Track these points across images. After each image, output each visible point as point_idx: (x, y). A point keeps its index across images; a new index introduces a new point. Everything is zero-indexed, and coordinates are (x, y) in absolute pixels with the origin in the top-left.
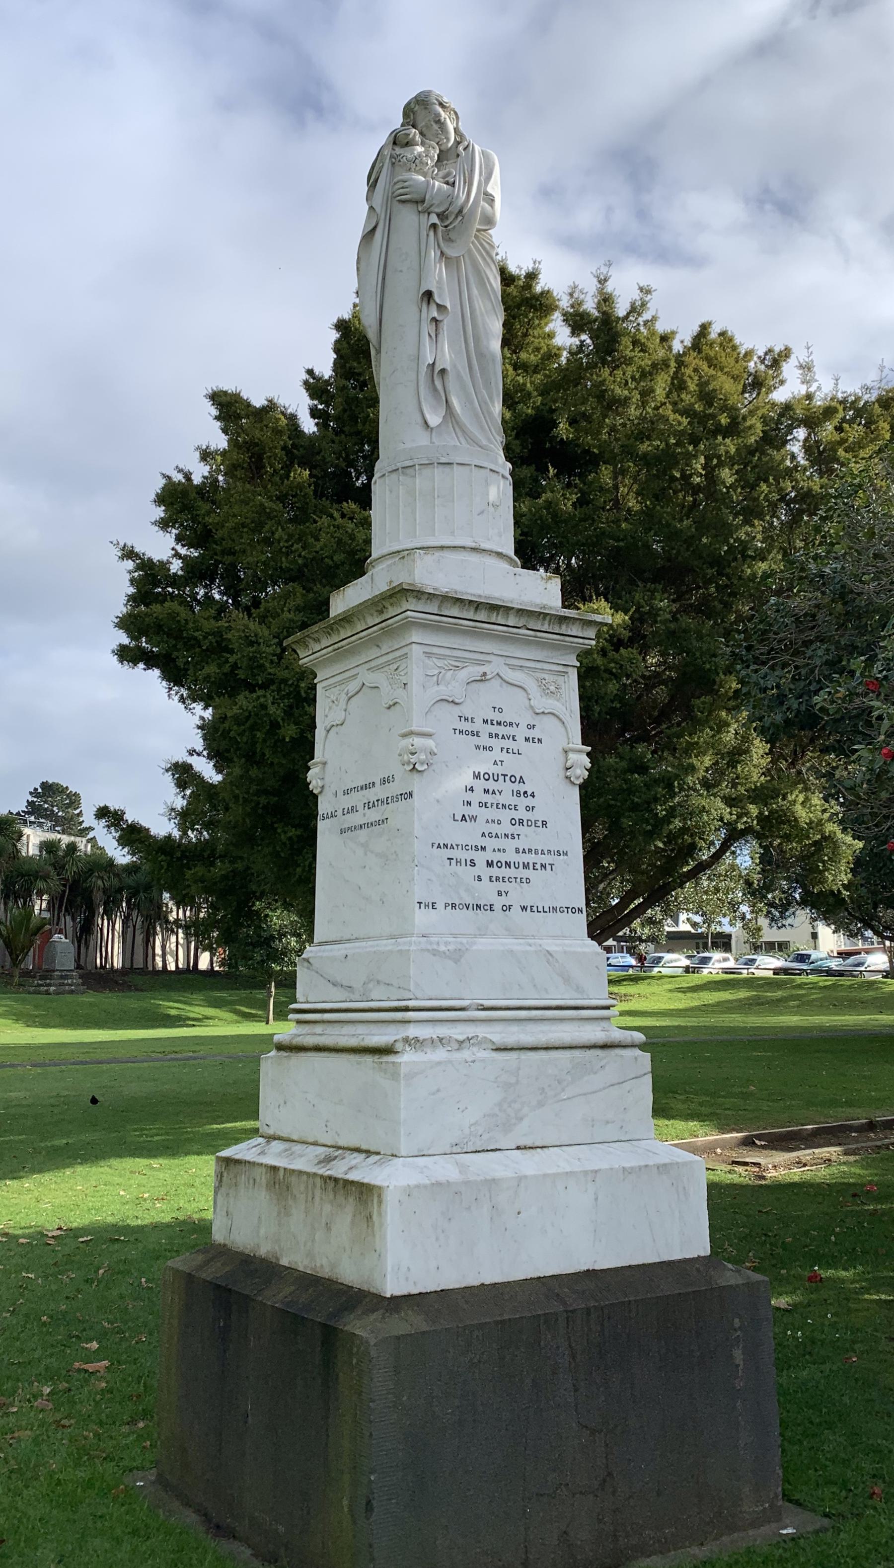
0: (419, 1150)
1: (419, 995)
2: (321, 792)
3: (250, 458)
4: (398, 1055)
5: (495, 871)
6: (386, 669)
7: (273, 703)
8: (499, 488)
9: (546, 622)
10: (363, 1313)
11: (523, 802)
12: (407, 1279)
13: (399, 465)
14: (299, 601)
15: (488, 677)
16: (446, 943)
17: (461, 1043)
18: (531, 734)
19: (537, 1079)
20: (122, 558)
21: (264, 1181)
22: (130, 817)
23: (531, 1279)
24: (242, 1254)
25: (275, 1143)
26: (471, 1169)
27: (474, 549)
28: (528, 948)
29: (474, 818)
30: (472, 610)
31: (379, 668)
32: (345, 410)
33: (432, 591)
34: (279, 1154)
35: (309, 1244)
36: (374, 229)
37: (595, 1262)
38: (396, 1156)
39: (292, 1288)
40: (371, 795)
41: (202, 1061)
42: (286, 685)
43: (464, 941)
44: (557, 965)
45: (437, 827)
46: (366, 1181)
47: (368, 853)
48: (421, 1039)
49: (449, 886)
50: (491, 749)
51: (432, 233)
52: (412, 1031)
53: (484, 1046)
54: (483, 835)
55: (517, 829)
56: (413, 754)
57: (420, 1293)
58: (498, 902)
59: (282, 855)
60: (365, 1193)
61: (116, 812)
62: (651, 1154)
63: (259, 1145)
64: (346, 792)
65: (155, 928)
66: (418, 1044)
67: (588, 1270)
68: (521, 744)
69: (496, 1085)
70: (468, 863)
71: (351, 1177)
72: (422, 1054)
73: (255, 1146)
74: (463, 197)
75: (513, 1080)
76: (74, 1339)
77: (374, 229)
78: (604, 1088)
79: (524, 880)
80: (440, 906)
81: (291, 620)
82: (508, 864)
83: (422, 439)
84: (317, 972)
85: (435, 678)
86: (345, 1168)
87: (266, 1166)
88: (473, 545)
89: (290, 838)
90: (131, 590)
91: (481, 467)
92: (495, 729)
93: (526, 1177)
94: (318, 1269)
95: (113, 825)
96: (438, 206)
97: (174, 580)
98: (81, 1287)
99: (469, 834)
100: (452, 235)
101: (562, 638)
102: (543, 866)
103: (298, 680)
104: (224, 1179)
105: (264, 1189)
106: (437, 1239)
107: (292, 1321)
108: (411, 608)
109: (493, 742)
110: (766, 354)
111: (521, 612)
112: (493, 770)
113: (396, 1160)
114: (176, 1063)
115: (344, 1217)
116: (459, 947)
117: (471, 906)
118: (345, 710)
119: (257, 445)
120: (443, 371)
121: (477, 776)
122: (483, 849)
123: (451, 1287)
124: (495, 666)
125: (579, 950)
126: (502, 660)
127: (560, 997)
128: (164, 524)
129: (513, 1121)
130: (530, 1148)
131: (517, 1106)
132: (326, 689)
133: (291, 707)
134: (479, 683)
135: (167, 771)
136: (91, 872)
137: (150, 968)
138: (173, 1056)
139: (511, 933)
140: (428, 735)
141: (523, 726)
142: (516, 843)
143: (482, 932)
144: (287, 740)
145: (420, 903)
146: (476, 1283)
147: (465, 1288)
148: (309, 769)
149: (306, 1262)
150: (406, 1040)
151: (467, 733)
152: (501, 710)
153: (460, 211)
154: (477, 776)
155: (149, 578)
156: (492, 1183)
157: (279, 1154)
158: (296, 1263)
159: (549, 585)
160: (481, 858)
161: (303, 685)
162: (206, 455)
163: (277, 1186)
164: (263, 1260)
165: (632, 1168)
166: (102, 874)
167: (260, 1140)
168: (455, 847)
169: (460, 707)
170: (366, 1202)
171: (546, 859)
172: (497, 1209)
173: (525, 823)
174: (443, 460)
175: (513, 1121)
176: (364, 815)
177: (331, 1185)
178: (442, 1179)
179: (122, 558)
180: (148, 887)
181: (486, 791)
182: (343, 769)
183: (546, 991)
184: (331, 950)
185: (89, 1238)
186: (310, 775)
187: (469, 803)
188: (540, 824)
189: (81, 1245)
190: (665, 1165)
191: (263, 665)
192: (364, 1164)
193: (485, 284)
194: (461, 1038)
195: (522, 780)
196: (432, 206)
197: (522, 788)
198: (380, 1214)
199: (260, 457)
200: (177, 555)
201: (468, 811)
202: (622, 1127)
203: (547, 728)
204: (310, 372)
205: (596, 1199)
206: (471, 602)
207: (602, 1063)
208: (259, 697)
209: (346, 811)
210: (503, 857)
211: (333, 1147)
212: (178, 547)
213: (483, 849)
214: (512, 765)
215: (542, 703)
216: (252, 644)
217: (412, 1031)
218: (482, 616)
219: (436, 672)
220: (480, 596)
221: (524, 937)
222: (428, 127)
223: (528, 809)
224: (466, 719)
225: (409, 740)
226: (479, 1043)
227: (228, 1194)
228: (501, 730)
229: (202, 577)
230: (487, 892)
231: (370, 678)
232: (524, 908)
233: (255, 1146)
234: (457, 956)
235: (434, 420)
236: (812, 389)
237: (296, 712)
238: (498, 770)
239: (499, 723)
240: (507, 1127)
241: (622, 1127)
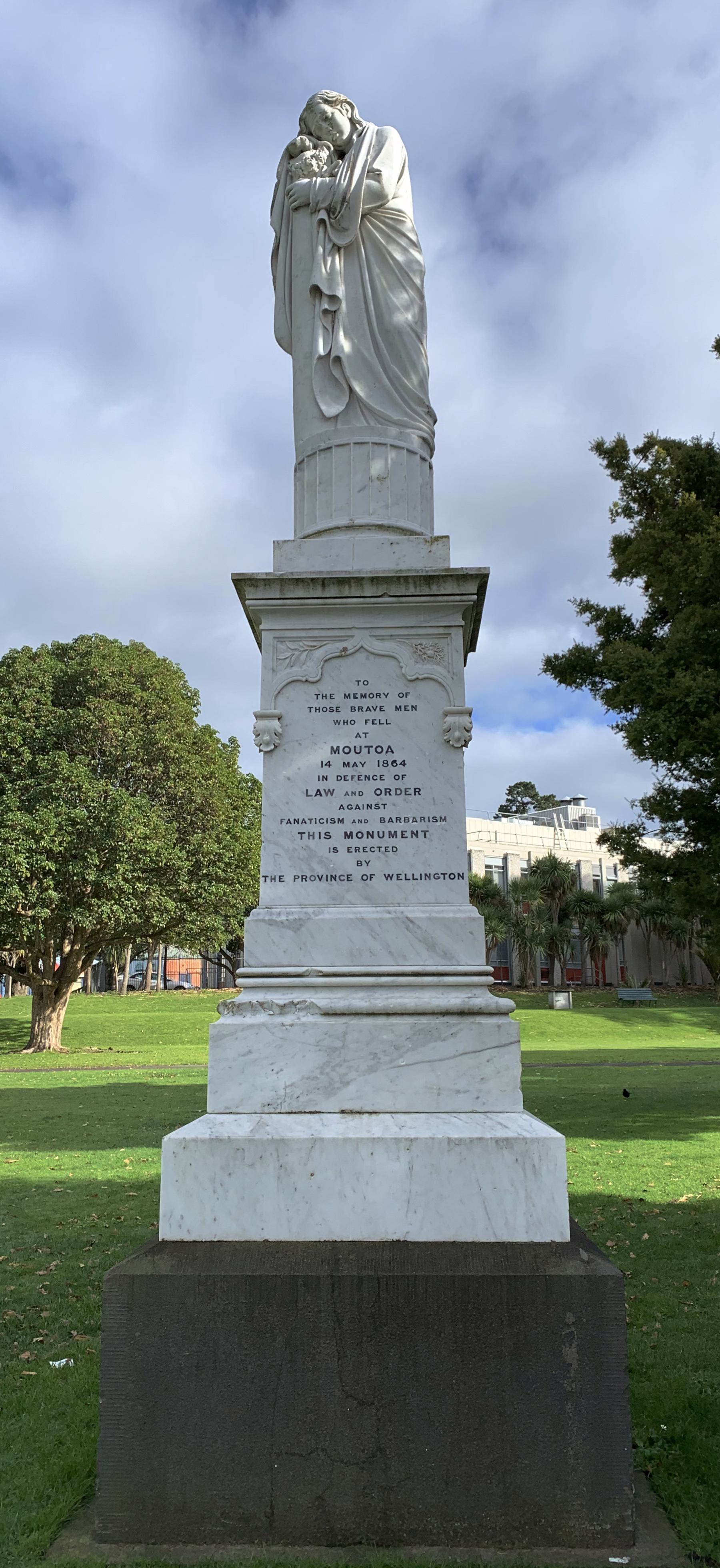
0: (226, 1108)
1: (252, 962)
5: (354, 842)
8: (386, 460)
18: (402, 702)
19: (367, 1044)
23: (325, 1241)
26: (267, 1128)
27: (350, 527)
29: (330, 792)
30: (319, 588)
33: (264, 577)
37: (407, 1233)
42: (675, 703)
44: (419, 931)
45: (287, 803)
49: (300, 859)
50: (352, 722)
51: (321, 230)
53: (312, 1011)
54: (341, 807)
57: (194, 1241)
58: (357, 873)
66: (235, 1009)
67: (398, 1241)
69: (318, 1048)
74: (344, 183)
75: (338, 1044)
78: (455, 1056)
79: (390, 849)
80: (288, 878)
82: (370, 835)
91: (362, 443)
92: (356, 703)
93: (322, 1139)
96: (324, 201)
99: (326, 808)
100: (344, 224)
101: (432, 599)
102: (415, 834)
106: (215, 1192)
109: (356, 715)
111: (375, 580)
112: (354, 742)
117: (325, 877)
121: (335, 751)
122: (341, 821)
123: (230, 1240)
126: (367, 632)
127: (422, 963)
131: (342, 1070)
134: (340, 659)
139: (371, 901)
142: (381, 813)
151: (324, 710)
152: (366, 682)
153: (344, 199)
154: (335, 751)
156: (281, 1144)
168: (308, 822)
169: (318, 685)
171: (419, 827)
172: (286, 1169)
173: (393, 792)
175: (337, 1085)
183: (404, 957)
187: (325, 778)
193: (387, 260)
194: (281, 1002)
195: (390, 749)
196: (317, 203)
197: (390, 758)
201: (322, 786)
202: (478, 1098)
206: (312, 579)
207: (453, 1030)
210: (364, 828)
213: (341, 821)
214: (377, 736)
218: (332, 591)
220: (321, 572)
221: (387, 904)
222: (320, 128)
223: (396, 777)
228: (366, 703)
230: (346, 863)
232: (389, 877)
234: (297, 925)
238: (362, 742)
239: (364, 696)
240: (330, 1090)
241: (478, 1098)
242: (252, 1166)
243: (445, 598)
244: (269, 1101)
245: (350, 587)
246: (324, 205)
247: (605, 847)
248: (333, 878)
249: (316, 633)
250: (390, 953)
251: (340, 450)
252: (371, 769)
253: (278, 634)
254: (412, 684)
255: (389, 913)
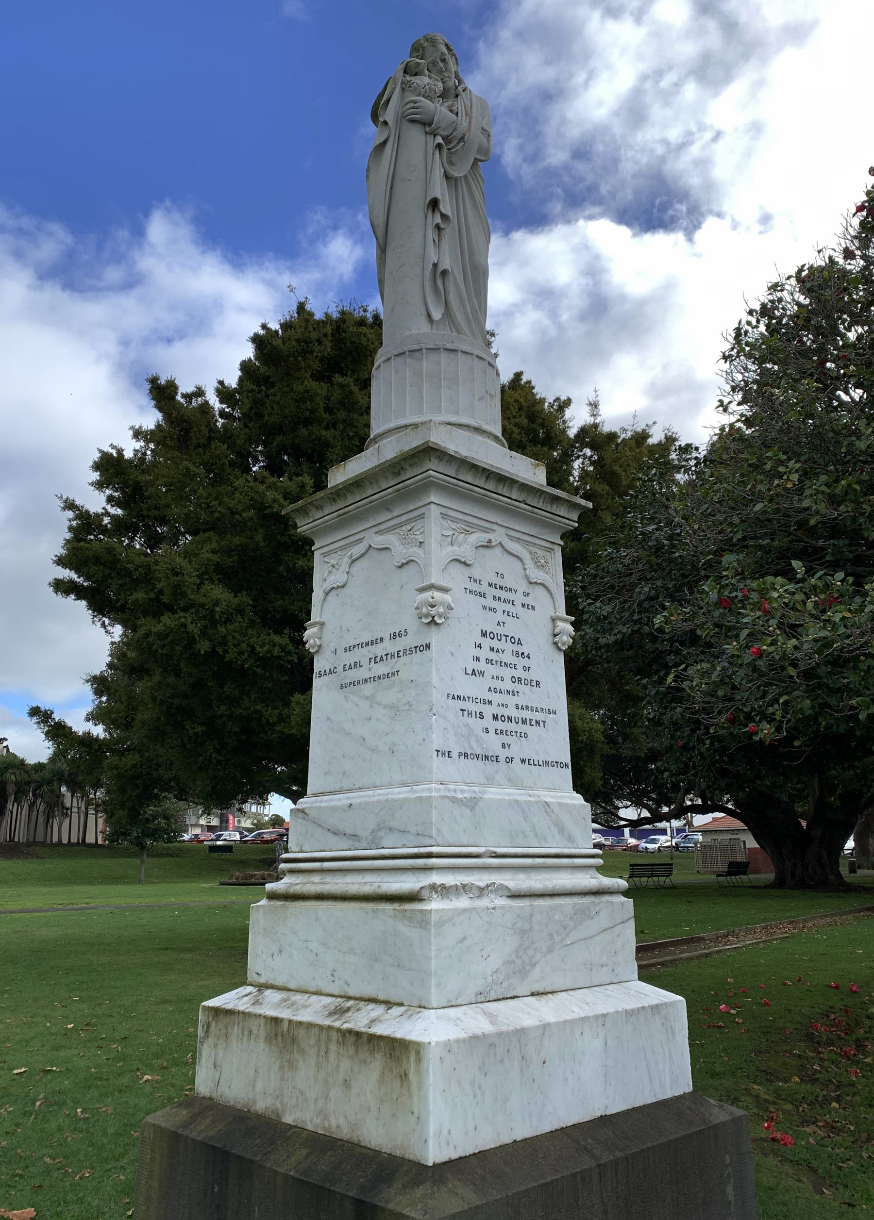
0: (449, 1001)
1: (441, 843)
2: (317, 652)
3: (180, 431)
4: (424, 903)
5: (500, 725)
6: (398, 530)
7: (192, 623)
9: (542, 500)
10: (405, 1187)
11: (521, 662)
12: (448, 1144)
13: (406, 348)
14: (214, 545)
15: (493, 544)
16: (462, 791)
17: (481, 889)
18: (526, 601)
20: (64, 509)
21: (262, 1032)
22: (57, 717)
23: (556, 1130)
24: (233, 1109)
25: (268, 992)
28: (530, 799)
29: (482, 673)
30: (483, 480)
31: (388, 530)
32: (251, 408)
33: (453, 453)
34: (278, 1005)
35: (321, 1103)
36: (385, 143)
38: (424, 1008)
39: (304, 1152)
40: (379, 650)
41: (95, 911)
43: (477, 789)
46: (399, 1035)
47: (375, 705)
48: (448, 885)
50: (494, 610)
51: (437, 152)
52: (436, 878)
55: (517, 687)
56: (433, 606)
57: (461, 1158)
58: (503, 754)
59: (189, 746)
60: (398, 1052)
61: (46, 711)
62: (642, 996)
63: (250, 994)
64: (348, 650)
65: (53, 812)
67: (601, 1116)
68: (518, 609)
70: (478, 715)
71: (379, 1030)
72: (448, 901)
73: (246, 995)
75: (527, 926)
76: (17, 1179)
77: (385, 143)
78: (599, 933)
80: (455, 754)
81: (209, 559)
82: (510, 719)
83: (425, 328)
84: (314, 822)
85: (449, 539)
86: (365, 1021)
87: (265, 1017)
88: (476, 425)
89: (196, 734)
90: (69, 536)
93: (549, 1024)
94: (333, 1130)
95: (42, 721)
96: (444, 130)
97: (104, 530)
98: (21, 1121)
100: (454, 159)
103: (214, 605)
104: (212, 1029)
105: (262, 1041)
106: (475, 1096)
107: (310, 1192)
108: (434, 469)
110: (555, 401)
113: (426, 1013)
114: (74, 912)
115: (370, 1075)
116: (473, 795)
118: (348, 573)
119: (186, 421)
120: (444, 273)
122: (490, 702)
124: (498, 536)
125: (569, 801)
126: (503, 530)
128: (100, 485)
129: (528, 967)
130: (542, 994)
131: (531, 952)
132: (324, 555)
133: (205, 627)
135: (87, 681)
136: (7, 768)
137: (49, 841)
138: (71, 906)
139: (513, 782)
140: (445, 590)
141: (520, 593)
143: (490, 781)
144: (202, 652)
145: (438, 751)
146: (509, 1141)
147: (500, 1146)
148: (305, 629)
149: (317, 1121)
150: (433, 887)
155: (85, 524)
157: (278, 1005)
158: (303, 1121)
159: (537, 472)
160: (488, 711)
161: (218, 609)
162: (138, 434)
163: (280, 1039)
164: (259, 1117)
165: (633, 1010)
166: (16, 771)
167: (249, 989)
170: (399, 1060)
171: (540, 716)
173: (523, 682)
174: (449, 346)
176: (370, 669)
177: (353, 1039)
178: (478, 1032)
179: (64, 509)
180: (50, 782)
181: (492, 649)
182: (344, 628)
184: (331, 800)
185: (23, 1070)
186: (307, 634)
188: (534, 683)
189: (15, 1077)
190: (657, 1006)
191: (185, 592)
192: (387, 1016)
194: (482, 884)
195: (520, 643)
196: (438, 128)
198: (419, 1072)
199: (187, 431)
200: (107, 514)
203: (539, 596)
204: (221, 383)
205: (606, 1043)
207: (598, 909)
208: (180, 618)
209: (347, 667)
210: (507, 712)
211: (341, 997)
212: (108, 507)
213: (490, 702)
214: (512, 628)
215: (537, 575)
216: (177, 574)
217: (436, 878)
218: (491, 486)
219: (451, 533)
224: (475, 581)
225: (427, 595)
226: (497, 890)
227: (216, 1045)
228: (503, 594)
229: (127, 530)
230: (493, 744)
231: (379, 541)
232: (523, 761)
233: (246, 995)
234: (472, 803)
235: (437, 315)
236: (597, 421)
237: (210, 632)
239: (501, 588)
240: (523, 973)
242: (502, 1061)
243: (560, 519)
244: (480, 989)
245: (504, 486)
246: (443, 133)
247: (35, 719)
248: (487, 757)
249: (470, 519)
250: (536, 835)
251: (464, 356)
252: (507, 657)
253: (444, 511)
254: (532, 586)
255: (530, 796)
